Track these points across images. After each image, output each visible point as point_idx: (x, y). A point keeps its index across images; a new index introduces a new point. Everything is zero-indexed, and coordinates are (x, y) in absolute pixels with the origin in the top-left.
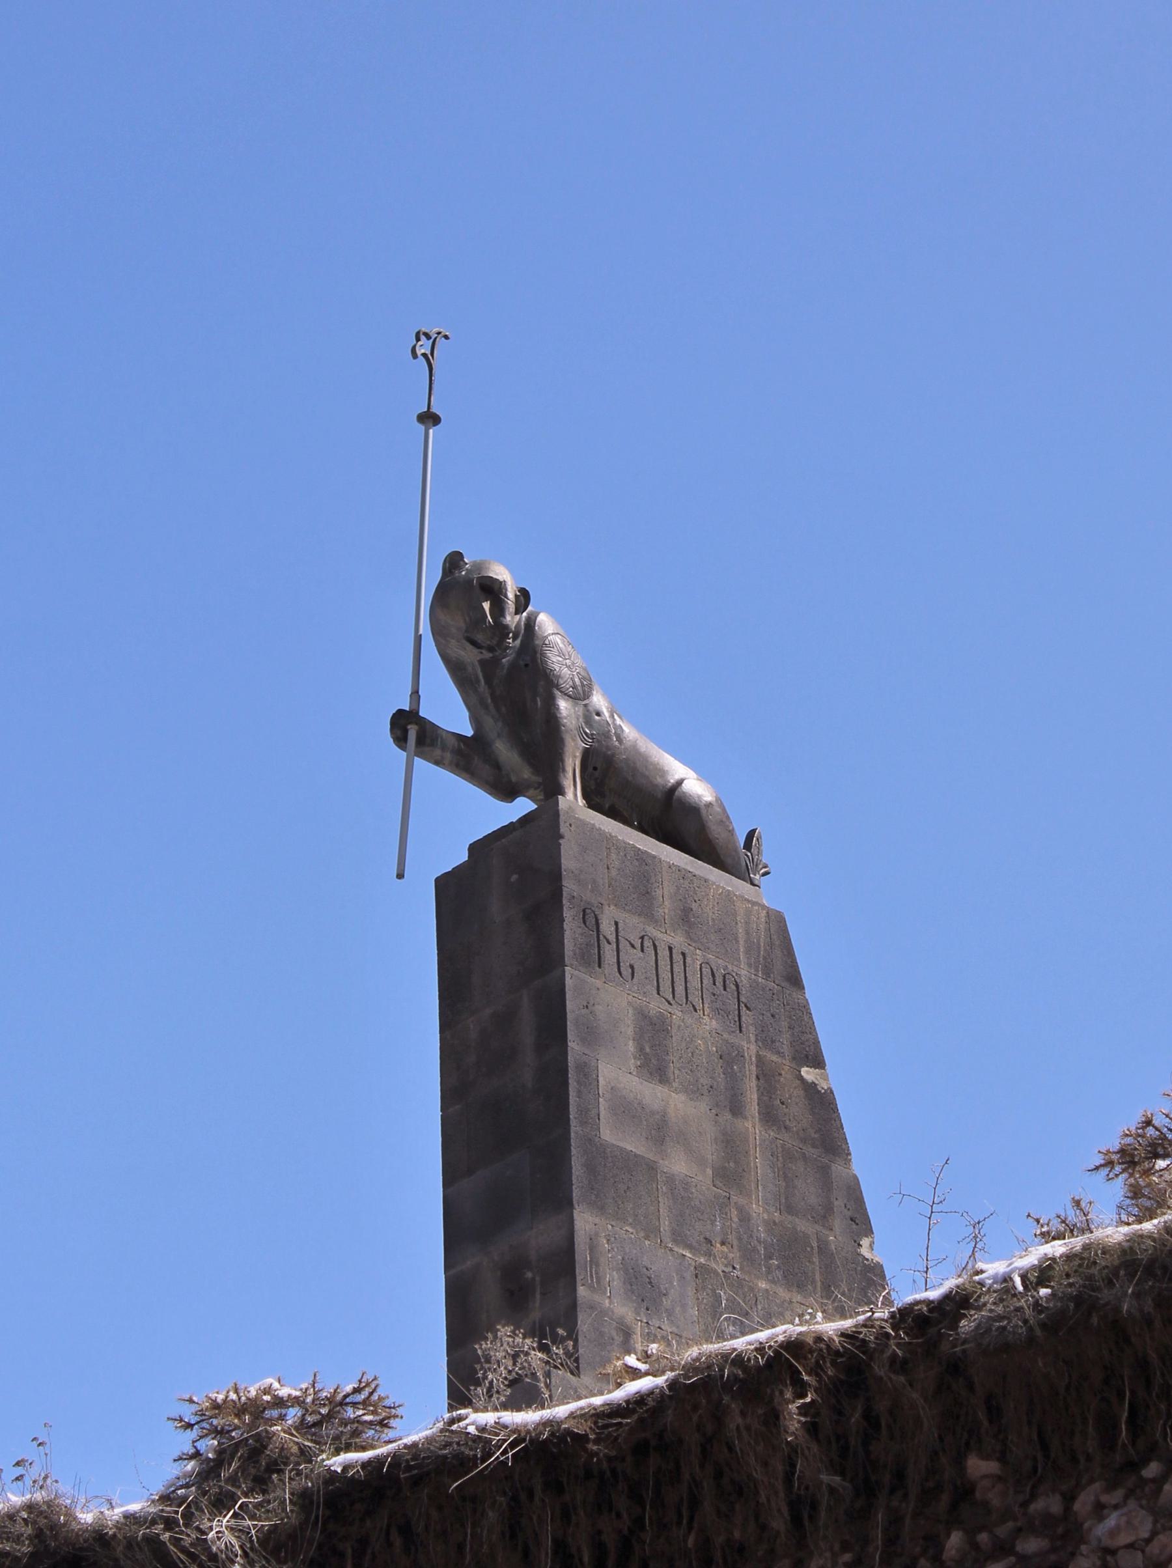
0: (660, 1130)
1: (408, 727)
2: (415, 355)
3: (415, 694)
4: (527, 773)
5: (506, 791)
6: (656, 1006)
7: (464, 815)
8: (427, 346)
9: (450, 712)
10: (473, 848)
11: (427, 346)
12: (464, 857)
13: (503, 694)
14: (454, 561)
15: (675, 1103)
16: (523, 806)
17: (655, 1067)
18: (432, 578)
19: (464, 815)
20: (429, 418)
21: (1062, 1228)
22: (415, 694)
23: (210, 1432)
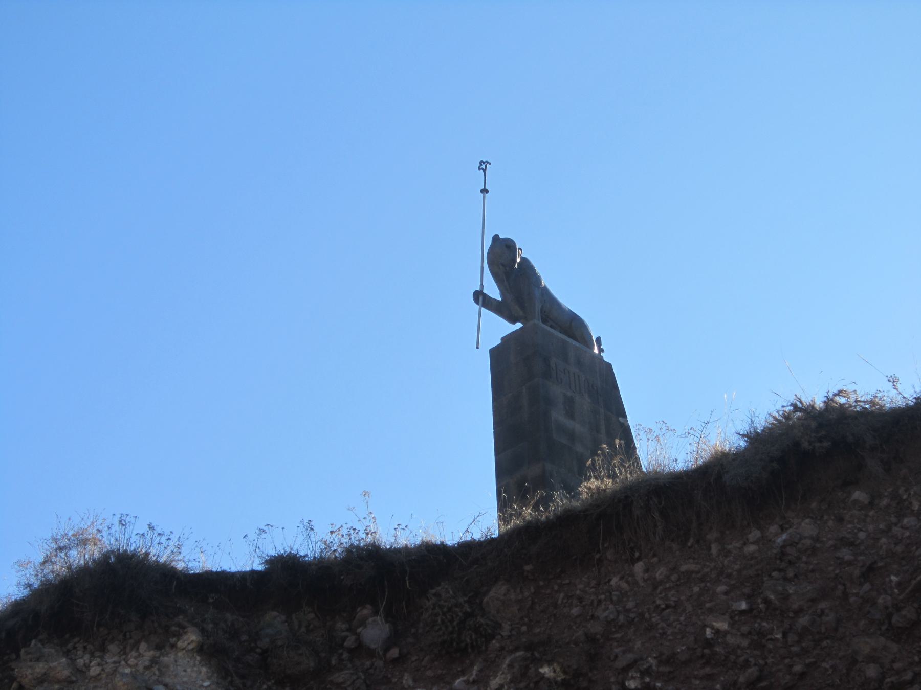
0: (572, 436)
1: (480, 297)
2: (480, 169)
3: (482, 285)
4: (521, 313)
5: (513, 320)
6: (569, 394)
7: (499, 328)
8: (483, 166)
9: (493, 291)
10: (502, 339)
11: (483, 166)
12: (500, 342)
13: (514, 281)
14: (496, 238)
15: (578, 427)
16: (519, 325)
17: (571, 415)
18: (488, 243)
19: (499, 328)
20: (485, 191)
21: (155, 669)
22: (482, 285)
23: (619, 673)
